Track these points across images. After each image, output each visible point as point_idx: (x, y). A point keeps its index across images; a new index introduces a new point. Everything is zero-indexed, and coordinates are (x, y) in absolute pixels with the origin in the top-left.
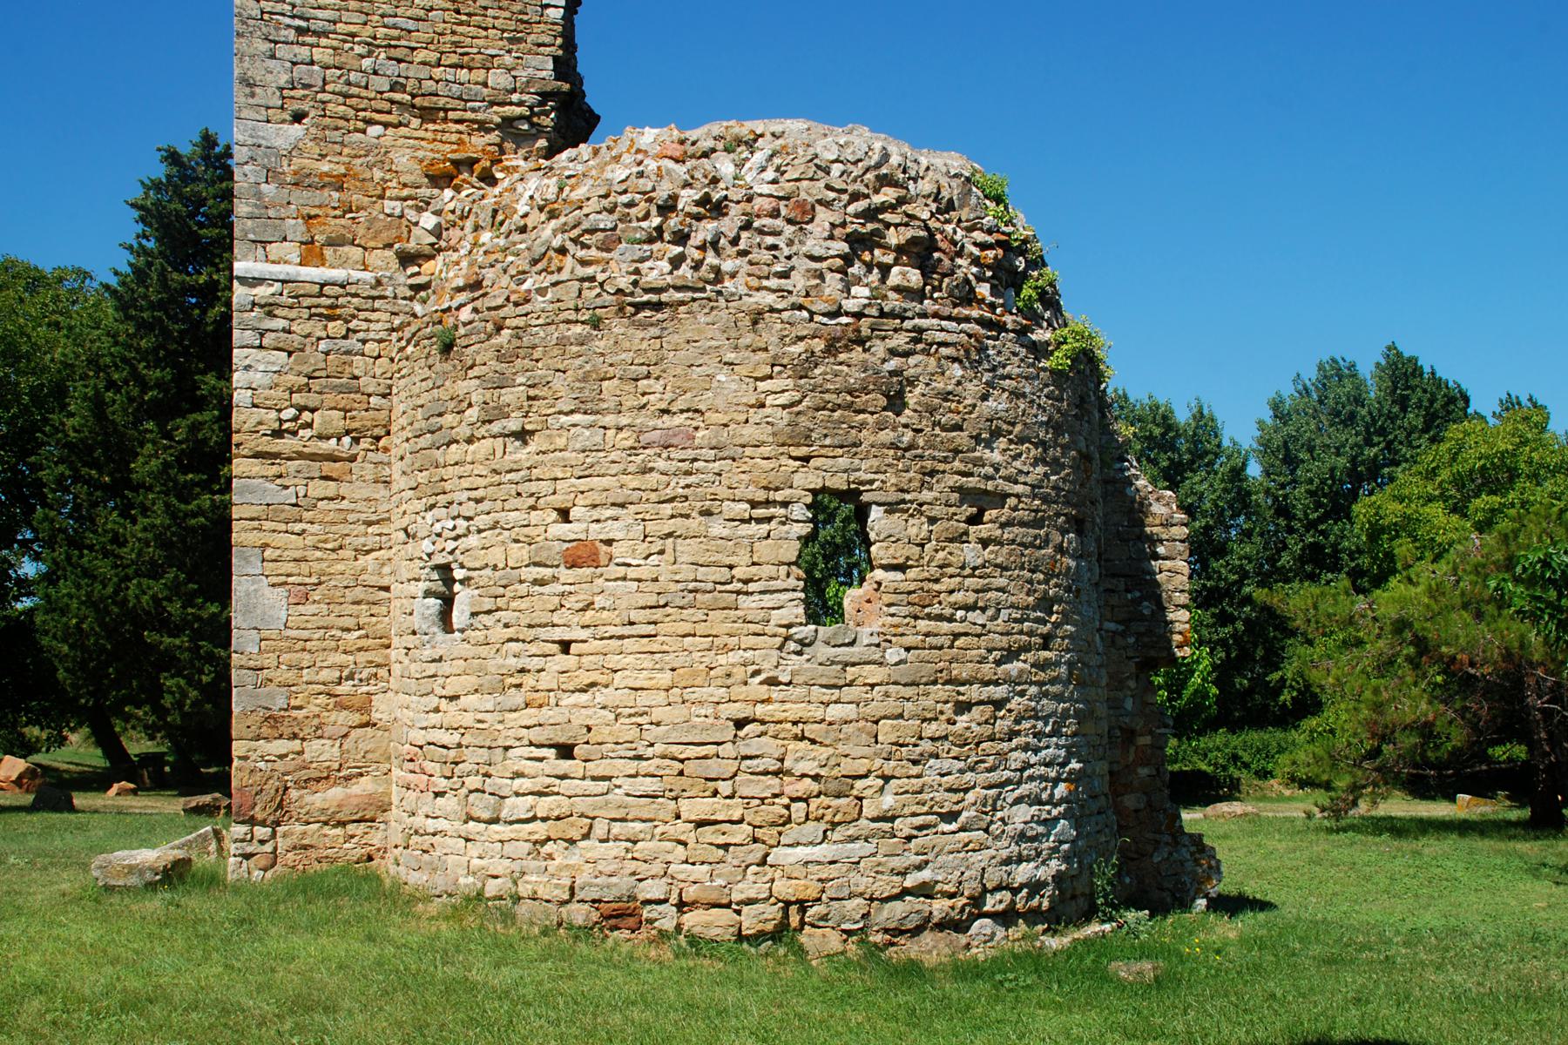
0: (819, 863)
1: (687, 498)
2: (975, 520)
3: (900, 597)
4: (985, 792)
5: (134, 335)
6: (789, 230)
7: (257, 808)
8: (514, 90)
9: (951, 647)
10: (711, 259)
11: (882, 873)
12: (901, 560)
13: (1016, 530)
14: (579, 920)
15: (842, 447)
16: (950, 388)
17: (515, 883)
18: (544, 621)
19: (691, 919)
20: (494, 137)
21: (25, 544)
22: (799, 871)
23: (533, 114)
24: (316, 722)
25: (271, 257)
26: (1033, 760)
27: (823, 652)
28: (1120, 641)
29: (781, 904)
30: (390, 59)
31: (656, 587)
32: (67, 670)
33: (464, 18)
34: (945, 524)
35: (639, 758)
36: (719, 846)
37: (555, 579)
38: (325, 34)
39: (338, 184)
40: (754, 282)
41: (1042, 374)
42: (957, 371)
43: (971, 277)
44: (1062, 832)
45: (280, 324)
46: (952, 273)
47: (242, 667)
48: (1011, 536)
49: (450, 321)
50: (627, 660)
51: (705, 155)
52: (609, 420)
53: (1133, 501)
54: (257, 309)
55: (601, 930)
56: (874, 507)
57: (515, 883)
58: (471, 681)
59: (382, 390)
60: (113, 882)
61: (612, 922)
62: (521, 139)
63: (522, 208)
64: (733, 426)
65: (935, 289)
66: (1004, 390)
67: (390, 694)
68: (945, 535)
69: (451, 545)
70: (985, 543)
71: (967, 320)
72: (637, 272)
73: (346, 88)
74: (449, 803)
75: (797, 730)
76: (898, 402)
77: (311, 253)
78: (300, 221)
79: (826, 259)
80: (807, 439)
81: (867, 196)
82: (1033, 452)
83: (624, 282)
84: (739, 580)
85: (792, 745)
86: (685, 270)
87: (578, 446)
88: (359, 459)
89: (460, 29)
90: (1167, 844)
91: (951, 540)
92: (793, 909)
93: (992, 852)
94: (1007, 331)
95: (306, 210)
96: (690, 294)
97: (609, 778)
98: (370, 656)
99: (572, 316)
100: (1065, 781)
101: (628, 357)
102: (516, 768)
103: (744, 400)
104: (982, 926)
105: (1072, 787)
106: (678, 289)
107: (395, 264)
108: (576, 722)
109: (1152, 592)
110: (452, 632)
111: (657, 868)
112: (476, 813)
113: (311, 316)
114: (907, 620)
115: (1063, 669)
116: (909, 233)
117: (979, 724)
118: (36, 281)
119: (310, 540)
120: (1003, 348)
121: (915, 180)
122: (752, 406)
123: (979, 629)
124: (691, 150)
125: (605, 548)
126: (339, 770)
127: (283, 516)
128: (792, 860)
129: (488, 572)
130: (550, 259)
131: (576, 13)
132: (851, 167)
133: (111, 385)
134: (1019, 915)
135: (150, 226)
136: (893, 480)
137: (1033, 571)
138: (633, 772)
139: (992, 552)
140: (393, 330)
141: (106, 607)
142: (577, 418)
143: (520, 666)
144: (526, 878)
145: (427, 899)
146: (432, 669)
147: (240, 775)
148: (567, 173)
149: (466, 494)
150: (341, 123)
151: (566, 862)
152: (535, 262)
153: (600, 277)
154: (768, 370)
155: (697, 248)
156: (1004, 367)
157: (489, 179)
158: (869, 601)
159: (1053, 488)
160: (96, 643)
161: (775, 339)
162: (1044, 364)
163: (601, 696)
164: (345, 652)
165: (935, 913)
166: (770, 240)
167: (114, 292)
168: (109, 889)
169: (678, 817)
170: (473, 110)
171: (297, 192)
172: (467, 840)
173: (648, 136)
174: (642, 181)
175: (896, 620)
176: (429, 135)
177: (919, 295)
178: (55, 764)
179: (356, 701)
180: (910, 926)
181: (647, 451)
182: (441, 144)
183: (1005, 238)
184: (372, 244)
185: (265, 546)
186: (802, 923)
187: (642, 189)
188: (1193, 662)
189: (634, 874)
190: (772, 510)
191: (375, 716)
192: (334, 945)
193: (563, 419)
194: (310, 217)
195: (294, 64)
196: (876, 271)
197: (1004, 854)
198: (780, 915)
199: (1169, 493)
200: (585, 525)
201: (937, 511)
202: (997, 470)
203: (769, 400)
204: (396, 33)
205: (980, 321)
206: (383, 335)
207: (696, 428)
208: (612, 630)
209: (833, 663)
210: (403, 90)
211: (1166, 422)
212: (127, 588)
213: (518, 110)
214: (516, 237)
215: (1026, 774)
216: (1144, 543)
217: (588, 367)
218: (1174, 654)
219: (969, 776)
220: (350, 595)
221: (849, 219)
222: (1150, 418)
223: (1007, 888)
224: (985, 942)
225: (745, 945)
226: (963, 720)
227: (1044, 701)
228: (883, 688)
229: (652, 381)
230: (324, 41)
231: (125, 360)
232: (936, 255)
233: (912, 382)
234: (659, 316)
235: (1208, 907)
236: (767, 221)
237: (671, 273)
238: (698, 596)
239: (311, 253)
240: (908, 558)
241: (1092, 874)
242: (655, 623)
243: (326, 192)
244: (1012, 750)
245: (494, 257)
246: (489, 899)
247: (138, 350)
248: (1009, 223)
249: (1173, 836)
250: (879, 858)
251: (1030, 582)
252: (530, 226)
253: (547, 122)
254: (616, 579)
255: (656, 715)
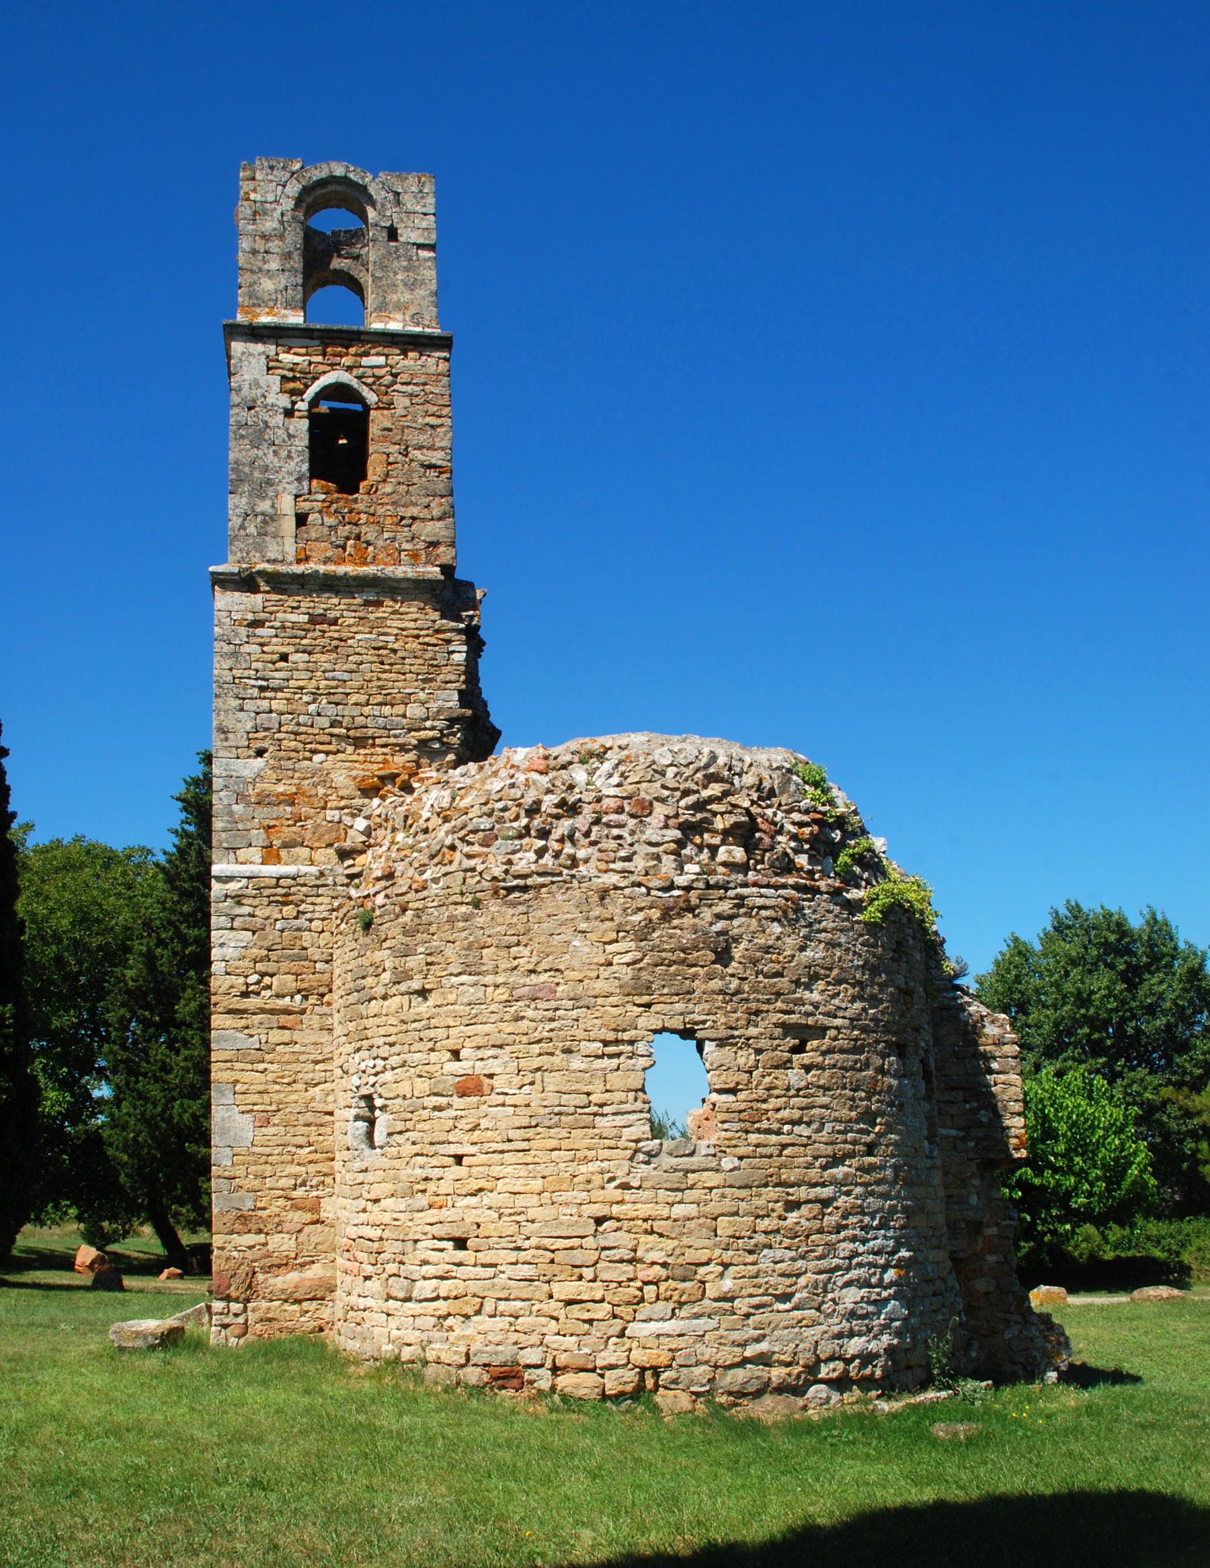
0: (669, 1336)
1: (551, 1040)
2: (799, 1049)
3: (732, 1115)
4: (816, 1276)
5: (178, 902)
6: (632, 822)
7: (232, 1288)
8: (428, 719)
9: (780, 1155)
10: (568, 849)
11: (724, 1344)
12: (732, 1085)
13: (836, 1056)
14: (473, 1381)
15: (677, 995)
16: (770, 943)
17: (424, 1349)
18: (442, 1139)
19: (564, 1381)
20: (412, 756)
21: (101, 1071)
22: (652, 1342)
23: (443, 735)
24: (277, 1220)
25: (240, 860)
26: (861, 1249)
27: (667, 1161)
28: (960, 1145)
29: (637, 1370)
30: (330, 703)
31: (528, 1111)
32: (127, 1175)
33: (387, 667)
34: (770, 1054)
35: (518, 1249)
36: (584, 1321)
37: (450, 1106)
38: (280, 689)
39: (291, 800)
40: (603, 866)
41: (856, 926)
42: (776, 928)
43: (789, 851)
44: (893, 1311)
45: (246, 910)
46: (772, 848)
47: (219, 1177)
48: (832, 1062)
49: (369, 905)
50: (507, 1170)
51: (564, 767)
52: (489, 979)
53: (967, 1024)
54: (229, 900)
55: (492, 1389)
56: (707, 1042)
57: (424, 1349)
58: (388, 1187)
59: (325, 957)
60: (124, 1344)
61: (500, 1382)
62: (433, 755)
63: (425, 814)
64: (586, 981)
65: (757, 862)
66: (820, 942)
67: (334, 1197)
68: (770, 1063)
69: (372, 1080)
70: (807, 1068)
71: (784, 886)
72: (510, 862)
73: (296, 728)
74: (374, 1285)
75: (647, 1226)
76: (726, 956)
77: (270, 855)
78: (262, 831)
79: (662, 844)
80: (648, 989)
81: (697, 792)
82: (850, 991)
83: (497, 871)
84: (595, 1105)
85: (643, 1238)
86: (548, 859)
87: (465, 1000)
88: (308, 1012)
89: (384, 676)
90: (1018, 1323)
91: (777, 1067)
92: (648, 1374)
93: (824, 1327)
94: (821, 893)
95: (266, 822)
96: (550, 878)
97: (495, 1265)
98: (318, 1167)
99: (458, 898)
100: (894, 1267)
101: (502, 929)
102: (423, 1257)
103: (595, 960)
104: (817, 1391)
105: (902, 1273)
106: (540, 874)
107: (335, 858)
108: (468, 1220)
109: (989, 1102)
110: (374, 1148)
111: (535, 1339)
112: (395, 1293)
113: (270, 902)
114: (738, 1134)
115: (889, 1172)
116: (731, 820)
117: (808, 1220)
118: (109, 859)
119: (270, 1077)
120: (819, 908)
121: (740, 775)
122: (602, 965)
123: (805, 1140)
124: (552, 763)
125: (487, 1081)
126: (295, 1259)
127: (249, 1058)
128: (646, 1333)
129: (399, 1101)
130: (444, 855)
131: (480, 656)
132: (683, 769)
133: (161, 943)
134: (853, 1382)
135: (191, 814)
136: (723, 1020)
137: (855, 1090)
138: (514, 1260)
139: (814, 1076)
140: (334, 910)
141: (156, 1124)
142: (464, 978)
143: (424, 1176)
144: (432, 1346)
145: (357, 1363)
146: (361, 1177)
147: (219, 1262)
148: (458, 786)
149: (383, 1040)
150: (293, 754)
151: (462, 1333)
152: (432, 857)
153: (480, 868)
154: (614, 935)
155: (557, 841)
156: (820, 922)
157: (407, 789)
158: (707, 1119)
159: (871, 1020)
160: (149, 1153)
161: (619, 911)
162: (859, 917)
163: (487, 1199)
164: (299, 1164)
165: (774, 1379)
166: (615, 832)
167: (163, 869)
168: (122, 1349)
169: (551, 1297)
170: (395, 736)
171: (259, 809)
172: (388, 1315)
173: (520, 755)
174: (513, 791)
175: (729, 1134)
176: (361, 758)
177: (744, 868)
178: (128, 1253)
179: (308, 1203)
180: (751, 1390)
181: (519, 1003)
182: (370, 764)
183: (819, 816)
184: (317, 845)
185: (236, 1082)
186: (657, 1386)
187: (513, 796)
188: (1130, 1155)
189: (516, 1343)
190: (621, 1047)
191: (323, 1215)
192: (277, 1396)
193: (454, 979)
194: (269, 827)
195: (258, 713)
196: (706, 850)
197: (836, 1329)
198: (637, 1378)
199: (1003, 1016)
200: (471, 1063)
201: (762, 1044)
202: (817, 1008)
203: (616, 960)
204: (334, 683)
205: (796, 887)
206: (325, 914)
207: (558, 984)
208: (495, 1146)
209: (676, 1170)
210: (340, 724)
211: (1121, 928)
212: (173, 1107)
213: (431, 734)
214: (421, 837)
215: (855, 1261)
216: (978, 1060)
217: (471, 939)
218: (1011, 1155)
219: (800, 1263)
220: (302, 1119)
221: (681, 811)
222: (1104, 926)
223: (840, 1358)
224: (821, 1405)
225: (609, 1404)
226: (793, 1217)
227: (871, 1199)
228: (720, 1191)
229: (521, 948)
230: (280, 695)
231: (170, 923)
232: (758, 835)
233: (737, 940)
234: (526, 896)
235: (1059, 1379)
236: (613, 817)
237: (536, 861)
238: (563, 1118)
239: (270, 855)
240: (738, 1083)
241: (928, 1347)
242: (528, 1140)
243: (281, 808)
244: (840, 1241)
245: (403, 853)
246: (403, 1363)
247: (181, 913)
248: (831, 802)
249: (1023, 1315)
250: (722, 1332)
251: (853, 1099)
252: (431, 828)
253: (454, 740)
254: (497, 1106)
255: (532, 1214)
